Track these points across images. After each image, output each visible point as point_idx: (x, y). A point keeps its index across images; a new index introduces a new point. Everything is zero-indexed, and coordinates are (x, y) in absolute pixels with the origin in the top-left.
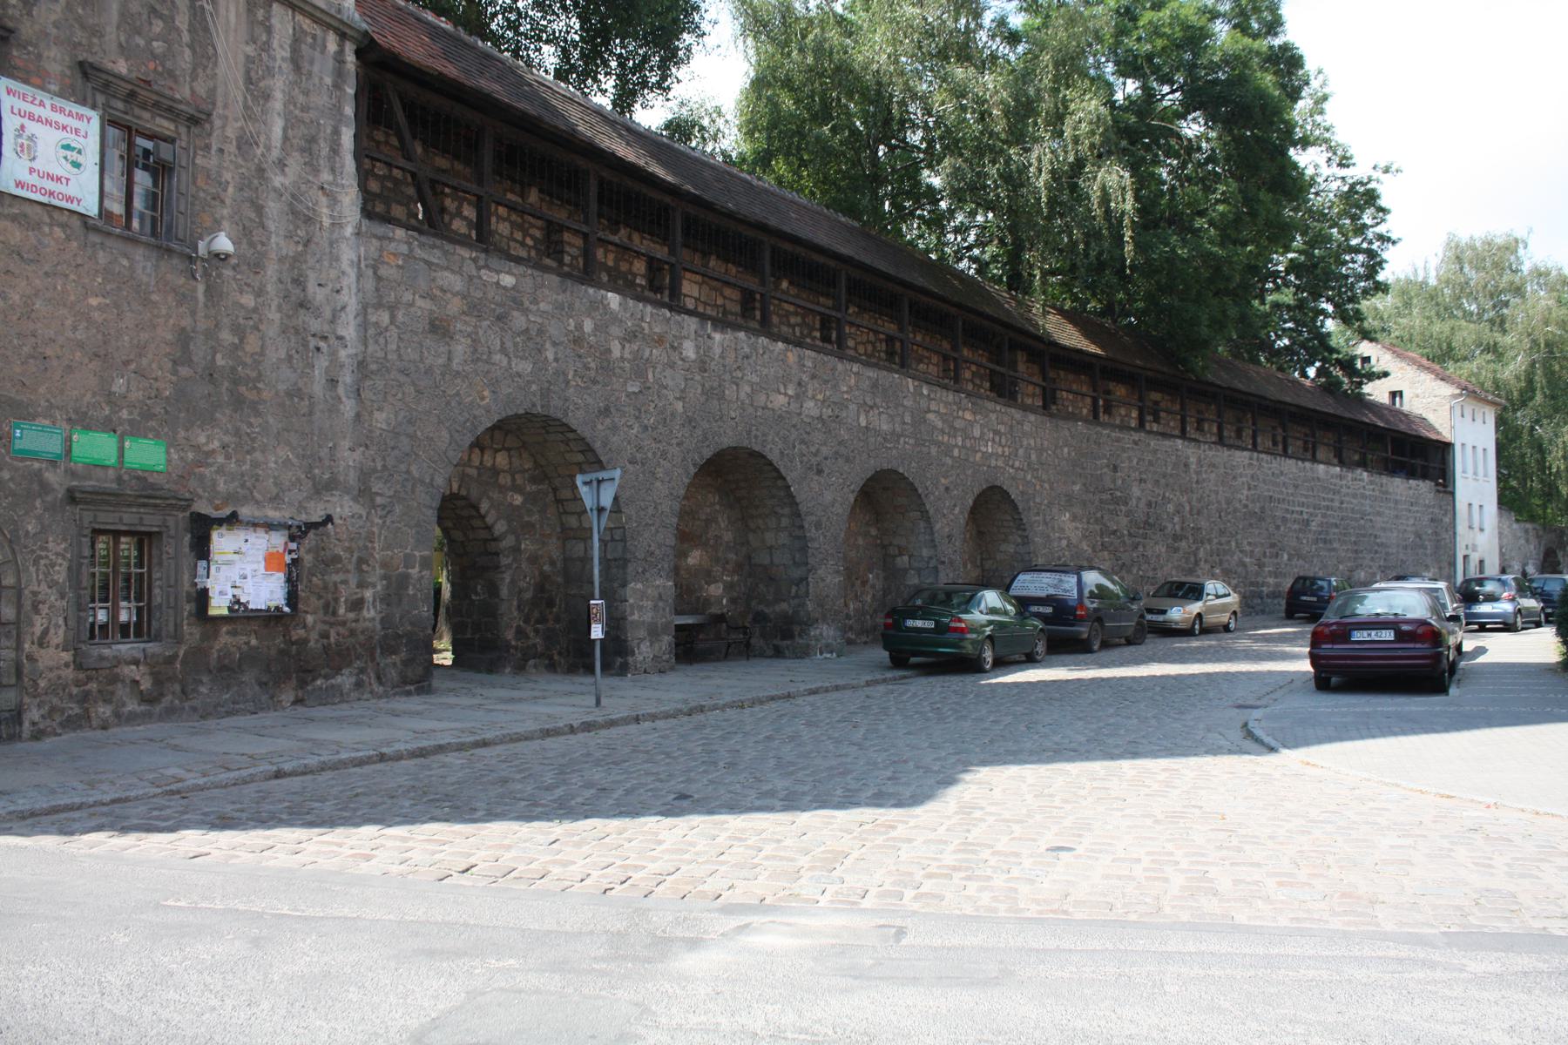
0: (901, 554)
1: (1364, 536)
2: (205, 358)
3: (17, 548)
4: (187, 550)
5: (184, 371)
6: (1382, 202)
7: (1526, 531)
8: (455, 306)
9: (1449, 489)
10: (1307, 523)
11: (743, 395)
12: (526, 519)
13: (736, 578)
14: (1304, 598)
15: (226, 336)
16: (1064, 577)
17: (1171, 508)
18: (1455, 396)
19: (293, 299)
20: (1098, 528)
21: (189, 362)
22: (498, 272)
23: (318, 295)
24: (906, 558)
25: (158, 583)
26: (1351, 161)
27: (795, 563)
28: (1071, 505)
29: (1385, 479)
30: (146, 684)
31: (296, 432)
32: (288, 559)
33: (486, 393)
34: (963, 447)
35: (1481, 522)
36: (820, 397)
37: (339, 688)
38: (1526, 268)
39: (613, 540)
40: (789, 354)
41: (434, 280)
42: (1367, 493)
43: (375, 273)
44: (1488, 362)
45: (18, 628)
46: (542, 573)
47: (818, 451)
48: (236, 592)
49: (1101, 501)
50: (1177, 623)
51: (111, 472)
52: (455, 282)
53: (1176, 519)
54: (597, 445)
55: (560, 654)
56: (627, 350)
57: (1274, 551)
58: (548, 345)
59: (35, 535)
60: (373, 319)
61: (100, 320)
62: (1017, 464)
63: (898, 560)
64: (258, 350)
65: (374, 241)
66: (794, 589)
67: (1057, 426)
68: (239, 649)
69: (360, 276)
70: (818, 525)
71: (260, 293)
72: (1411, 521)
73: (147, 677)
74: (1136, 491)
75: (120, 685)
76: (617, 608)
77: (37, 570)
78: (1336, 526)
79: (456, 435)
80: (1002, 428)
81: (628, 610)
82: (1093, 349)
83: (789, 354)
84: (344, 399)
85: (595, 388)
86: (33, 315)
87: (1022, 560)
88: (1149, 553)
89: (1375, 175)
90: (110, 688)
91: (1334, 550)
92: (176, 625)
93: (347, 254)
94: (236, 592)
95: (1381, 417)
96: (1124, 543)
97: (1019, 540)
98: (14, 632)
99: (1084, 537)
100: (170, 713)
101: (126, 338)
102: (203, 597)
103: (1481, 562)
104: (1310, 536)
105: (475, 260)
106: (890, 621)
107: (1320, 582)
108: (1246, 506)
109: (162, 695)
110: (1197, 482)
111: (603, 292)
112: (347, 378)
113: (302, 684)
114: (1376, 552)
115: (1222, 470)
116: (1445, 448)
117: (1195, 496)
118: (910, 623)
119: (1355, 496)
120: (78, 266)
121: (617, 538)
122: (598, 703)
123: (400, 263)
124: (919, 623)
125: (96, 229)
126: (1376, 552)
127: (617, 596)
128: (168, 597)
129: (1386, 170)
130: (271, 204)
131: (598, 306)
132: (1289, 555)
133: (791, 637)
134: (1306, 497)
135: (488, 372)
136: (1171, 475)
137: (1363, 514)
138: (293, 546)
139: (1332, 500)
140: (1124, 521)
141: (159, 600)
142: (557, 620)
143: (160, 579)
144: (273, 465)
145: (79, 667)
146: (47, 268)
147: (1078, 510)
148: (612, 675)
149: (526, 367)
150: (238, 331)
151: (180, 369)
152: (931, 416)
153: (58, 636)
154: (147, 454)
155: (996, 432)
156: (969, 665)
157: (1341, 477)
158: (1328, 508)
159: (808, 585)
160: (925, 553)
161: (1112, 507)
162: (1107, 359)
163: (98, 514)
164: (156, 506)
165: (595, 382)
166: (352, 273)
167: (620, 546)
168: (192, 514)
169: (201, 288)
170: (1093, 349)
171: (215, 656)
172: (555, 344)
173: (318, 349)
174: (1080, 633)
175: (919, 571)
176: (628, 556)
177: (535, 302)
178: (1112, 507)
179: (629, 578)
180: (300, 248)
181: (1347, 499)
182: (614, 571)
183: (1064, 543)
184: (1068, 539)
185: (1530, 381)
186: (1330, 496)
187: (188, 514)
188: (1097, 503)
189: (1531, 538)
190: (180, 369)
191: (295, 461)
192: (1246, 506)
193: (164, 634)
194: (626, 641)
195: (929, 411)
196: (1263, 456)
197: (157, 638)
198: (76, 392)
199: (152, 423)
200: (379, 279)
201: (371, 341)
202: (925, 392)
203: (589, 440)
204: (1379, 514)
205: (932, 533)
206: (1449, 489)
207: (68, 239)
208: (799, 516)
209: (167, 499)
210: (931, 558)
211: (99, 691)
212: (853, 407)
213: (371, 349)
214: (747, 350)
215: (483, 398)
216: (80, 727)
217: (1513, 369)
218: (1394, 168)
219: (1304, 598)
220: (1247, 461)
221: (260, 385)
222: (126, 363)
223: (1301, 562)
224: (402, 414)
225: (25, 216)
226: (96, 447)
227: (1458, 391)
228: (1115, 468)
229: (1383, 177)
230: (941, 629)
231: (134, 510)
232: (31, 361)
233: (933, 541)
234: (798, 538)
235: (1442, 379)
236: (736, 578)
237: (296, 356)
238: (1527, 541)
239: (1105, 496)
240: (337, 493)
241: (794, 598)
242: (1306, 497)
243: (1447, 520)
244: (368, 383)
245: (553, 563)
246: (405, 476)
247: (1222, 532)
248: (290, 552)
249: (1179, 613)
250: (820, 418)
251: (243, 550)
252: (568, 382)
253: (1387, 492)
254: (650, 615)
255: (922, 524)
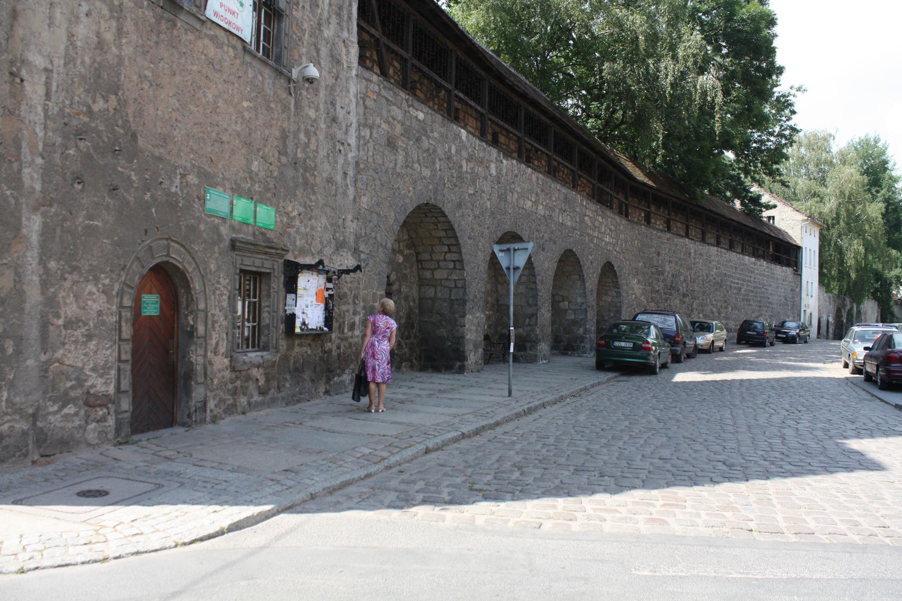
0: (563, 300)
1: (763, 298)
2: (292, 151)
3: (206, 281)
4: (282, 286)
5: (284, 159)
6: (795, 109)
7: (830, 298)
8: (399, 129)
9: (799, 273)
10: (740, 289)
11: (514, 200)
12: (404, 272)
13: (491, 312)
14: (749, 333)
15: (302, 136)
16: (668, 318)
17: (682, 278)
18: (804, 221)
19: (331, 115)
20: (649, 288)
21: (286, 154)
22: (417, 110)
23: (341, 113)
24: (566, 303)
25: (266, 309)
26: (779, 83)
27: (528, 304)
28: (638, 275)
29: (773, 266)
30: (262, 382)
31: (330, 207)
32: (326, 294)
33: (411, 188)
34: (598, 237)
35: (812, 292)
36: (544, 203)
37: (342, 382)
38: (835, 150)
39: (456, 287)
40: (533, 176)
41: (389, 111)
42: (766, 273)
43: (364, 103)
44: (817, 202)
45: (205, 341)
46: (410, 307)
47: (543, 236)
48: (304, 316)
49: (652, 273)
50: (702, 346)
51: (250, 228)
52: (397, 112)
53: (684, 285)
54: (456, 226)
55: (416, 359)
56: (469, 167)
57: (726, 304)
58: (437, 160)
59: (214, 272)
60: (363, 134)
61: (248, 118)
62: (618, 249)
63: (561, 305)
64: (315, 149)
65: (364, 81)
66: (527, 320)
67: (633, 228)
68: (303, 356)
69: (357, 104)
70: (542, 282)
71: (317, 109)
72: (783, 291)
73: (263, 376)
74: (667, 268)
75: (251, 383)
76: (457, 331)
77: (215, 298)
78: (752, 291)
79: (397, 215)
80: (613, 227)
81: (466, 332)
82: (650, 183)
83: (533, 176)
84: (350, 186)
85: (457, 189)
86: (218, 110)
87: (616, 306)
88: (672, 304)
89: (793, 92)
90: (246, 384)
91: (750, 305)
92: (276, 339)
93: (353, 89)
94: (304, 316)
95: (771, 230)
96: (661, 297)
97: (615, 294)
98: (204, 343)
99: (643, 293)
100: (274, 400)
101: (259, 132)
102: (291, 319)
103: (811, 314)
104: (741, 297)
105: (407, 101)
106: (603, 342)
107: (755, 324)
108: (715, 278)
109: (269, 389)
110: (694, 264)
111: (460, 129)
112: (351, 173)
113: (328, 382)
114: (768, 307)
115: (705, 257)
116: (798, 249)
117: (693, 272)
118: (617, 344)
119: (760, 275)
120: (240, 77)
121: (459, 286)
122: (510, 394)
123: (375, 97)
124: (623, 344)
125: (250, 53)
126: (768, 307)
127: (458, 323)
128: (273, 319)
129: (799, 89)
130: (323, 48)
131: (457, 136)
132: (732, 307)
133: (525, 349)
134: (740, 274)
135: (412, 175)
136: (683, 259)
137: (764, 285)
138: (330, 285)
139: (751, 277)
140: (662, 284)
141: (267, 321)
142: (415, 337)
143: (269, 306)
144: (319, 229)
145: (233, 369)
146: (225, 77)
147: (640, 278)
148: (454, 373)
149: (427, 173)
150: (307, 133)
151: (281, 157)
152: (586, 218)
153: (222, 349)
154: (266, 216)
155: (611, 230)
156: (646, 369)
157: (755, 264)
158: (749, 281)
159: (537, 318)
160: (579, 300)
161: (656, 276)
162: (657, 190)
163: (245, 259)
164: (271, 254)
165: (456, 186)
166: (354, 100)
167: (462, 291)
168: (285, 260)
169: (293, 102)
170: (650, 183)
171: (292, 361)
172: (440, 160)
173: (340, 151)
174: (677, 350)
175: (575, 311)
176: (467, 298)
177: (432, 131)
178: (656, 276)
179: (467, 312)
180: (334, 81)
181: (757, 276)
182: (456, 307)
183: (634, 296)
184: (635, 294)
185: (838, 214)
186: (750, 274)
187: (282, 261)
188: (650, 274)
189: (832, 302)
190: (281, 157)
191: (329, 227)
192: (715, 278)
193: (271, 345)
194: (464, 352)
195: (586, 215)
196: (723, 250)
197: (265, 348)
198: (235, 169)
199: (269, 195)
200: (366, 107)
201: (361, 149)
202: (585, 204)
203: (452, 223)
204: (770, 286)
205: (585, 288)
206: (799, 273)
207: (235, 58)
208: (534, 276)
209: (277, 249)
210: (583, 303)
211: (241, 387)
212: (557, 210)
213: (361, 153)
214: (516, 172)
215: (409, 192)
216: (232, 413)
217: (830, 206)
218: (804, 88)
219: (749, 333)
220: (716, 253)
221: (316, 173)
222: (259, 150)
223: (737, 312)
224: (375, 199)
225: (216, 37)
226: (242, 208)
227: (806, 218)
228: (659, 254)
229: (797, 94)
230: (636, 348)
231: (260, 256)
232: (216, 143)
233: (585, 293)
234: (532, 289)
235: (797, 211)
236: (491, 312)
237: (331, 155)
238: (830, 303)
239: (654, 270)
240: (345, 250)
241: (527, 326)
242: (740, 274)
243: (798, 290)
244: (360, 177)
245: (414, 301)
246: (374, 241)
247: (704, 293)
248: (327, 289)
249: (703, 340)
250: (544, 216)
251: (307, 287)
252: (445, 184)
253: (773, 274)
254: (475, 335)
255: (579, 283)
